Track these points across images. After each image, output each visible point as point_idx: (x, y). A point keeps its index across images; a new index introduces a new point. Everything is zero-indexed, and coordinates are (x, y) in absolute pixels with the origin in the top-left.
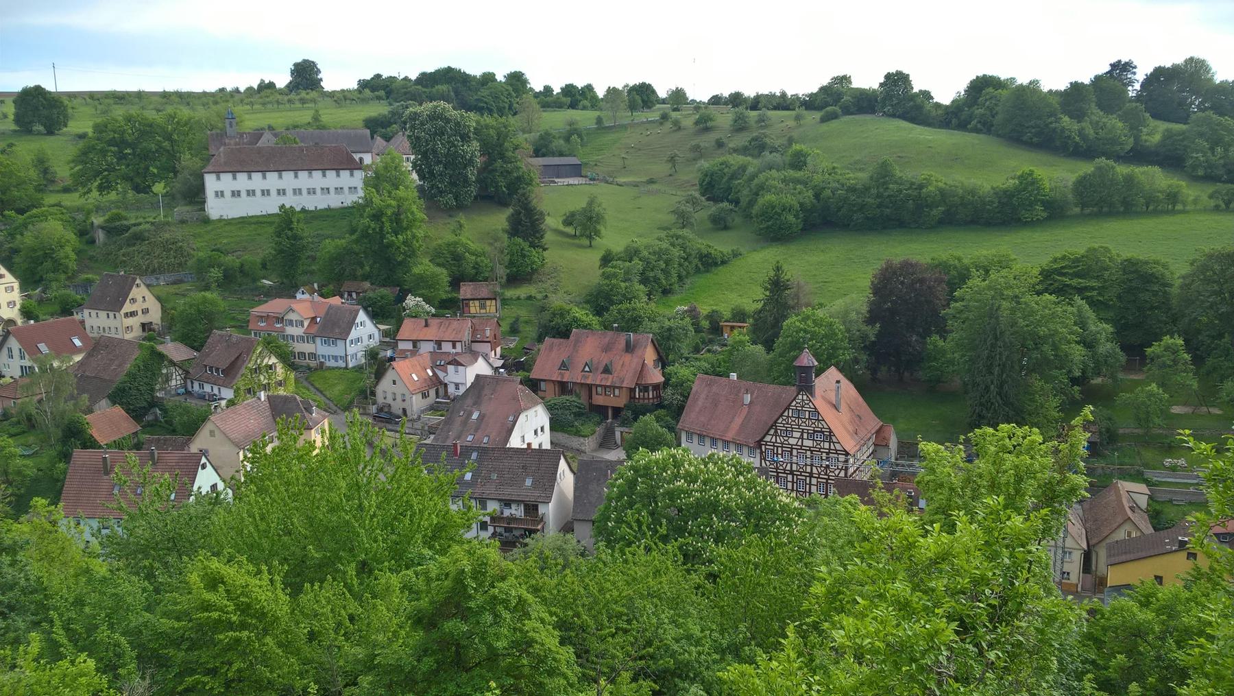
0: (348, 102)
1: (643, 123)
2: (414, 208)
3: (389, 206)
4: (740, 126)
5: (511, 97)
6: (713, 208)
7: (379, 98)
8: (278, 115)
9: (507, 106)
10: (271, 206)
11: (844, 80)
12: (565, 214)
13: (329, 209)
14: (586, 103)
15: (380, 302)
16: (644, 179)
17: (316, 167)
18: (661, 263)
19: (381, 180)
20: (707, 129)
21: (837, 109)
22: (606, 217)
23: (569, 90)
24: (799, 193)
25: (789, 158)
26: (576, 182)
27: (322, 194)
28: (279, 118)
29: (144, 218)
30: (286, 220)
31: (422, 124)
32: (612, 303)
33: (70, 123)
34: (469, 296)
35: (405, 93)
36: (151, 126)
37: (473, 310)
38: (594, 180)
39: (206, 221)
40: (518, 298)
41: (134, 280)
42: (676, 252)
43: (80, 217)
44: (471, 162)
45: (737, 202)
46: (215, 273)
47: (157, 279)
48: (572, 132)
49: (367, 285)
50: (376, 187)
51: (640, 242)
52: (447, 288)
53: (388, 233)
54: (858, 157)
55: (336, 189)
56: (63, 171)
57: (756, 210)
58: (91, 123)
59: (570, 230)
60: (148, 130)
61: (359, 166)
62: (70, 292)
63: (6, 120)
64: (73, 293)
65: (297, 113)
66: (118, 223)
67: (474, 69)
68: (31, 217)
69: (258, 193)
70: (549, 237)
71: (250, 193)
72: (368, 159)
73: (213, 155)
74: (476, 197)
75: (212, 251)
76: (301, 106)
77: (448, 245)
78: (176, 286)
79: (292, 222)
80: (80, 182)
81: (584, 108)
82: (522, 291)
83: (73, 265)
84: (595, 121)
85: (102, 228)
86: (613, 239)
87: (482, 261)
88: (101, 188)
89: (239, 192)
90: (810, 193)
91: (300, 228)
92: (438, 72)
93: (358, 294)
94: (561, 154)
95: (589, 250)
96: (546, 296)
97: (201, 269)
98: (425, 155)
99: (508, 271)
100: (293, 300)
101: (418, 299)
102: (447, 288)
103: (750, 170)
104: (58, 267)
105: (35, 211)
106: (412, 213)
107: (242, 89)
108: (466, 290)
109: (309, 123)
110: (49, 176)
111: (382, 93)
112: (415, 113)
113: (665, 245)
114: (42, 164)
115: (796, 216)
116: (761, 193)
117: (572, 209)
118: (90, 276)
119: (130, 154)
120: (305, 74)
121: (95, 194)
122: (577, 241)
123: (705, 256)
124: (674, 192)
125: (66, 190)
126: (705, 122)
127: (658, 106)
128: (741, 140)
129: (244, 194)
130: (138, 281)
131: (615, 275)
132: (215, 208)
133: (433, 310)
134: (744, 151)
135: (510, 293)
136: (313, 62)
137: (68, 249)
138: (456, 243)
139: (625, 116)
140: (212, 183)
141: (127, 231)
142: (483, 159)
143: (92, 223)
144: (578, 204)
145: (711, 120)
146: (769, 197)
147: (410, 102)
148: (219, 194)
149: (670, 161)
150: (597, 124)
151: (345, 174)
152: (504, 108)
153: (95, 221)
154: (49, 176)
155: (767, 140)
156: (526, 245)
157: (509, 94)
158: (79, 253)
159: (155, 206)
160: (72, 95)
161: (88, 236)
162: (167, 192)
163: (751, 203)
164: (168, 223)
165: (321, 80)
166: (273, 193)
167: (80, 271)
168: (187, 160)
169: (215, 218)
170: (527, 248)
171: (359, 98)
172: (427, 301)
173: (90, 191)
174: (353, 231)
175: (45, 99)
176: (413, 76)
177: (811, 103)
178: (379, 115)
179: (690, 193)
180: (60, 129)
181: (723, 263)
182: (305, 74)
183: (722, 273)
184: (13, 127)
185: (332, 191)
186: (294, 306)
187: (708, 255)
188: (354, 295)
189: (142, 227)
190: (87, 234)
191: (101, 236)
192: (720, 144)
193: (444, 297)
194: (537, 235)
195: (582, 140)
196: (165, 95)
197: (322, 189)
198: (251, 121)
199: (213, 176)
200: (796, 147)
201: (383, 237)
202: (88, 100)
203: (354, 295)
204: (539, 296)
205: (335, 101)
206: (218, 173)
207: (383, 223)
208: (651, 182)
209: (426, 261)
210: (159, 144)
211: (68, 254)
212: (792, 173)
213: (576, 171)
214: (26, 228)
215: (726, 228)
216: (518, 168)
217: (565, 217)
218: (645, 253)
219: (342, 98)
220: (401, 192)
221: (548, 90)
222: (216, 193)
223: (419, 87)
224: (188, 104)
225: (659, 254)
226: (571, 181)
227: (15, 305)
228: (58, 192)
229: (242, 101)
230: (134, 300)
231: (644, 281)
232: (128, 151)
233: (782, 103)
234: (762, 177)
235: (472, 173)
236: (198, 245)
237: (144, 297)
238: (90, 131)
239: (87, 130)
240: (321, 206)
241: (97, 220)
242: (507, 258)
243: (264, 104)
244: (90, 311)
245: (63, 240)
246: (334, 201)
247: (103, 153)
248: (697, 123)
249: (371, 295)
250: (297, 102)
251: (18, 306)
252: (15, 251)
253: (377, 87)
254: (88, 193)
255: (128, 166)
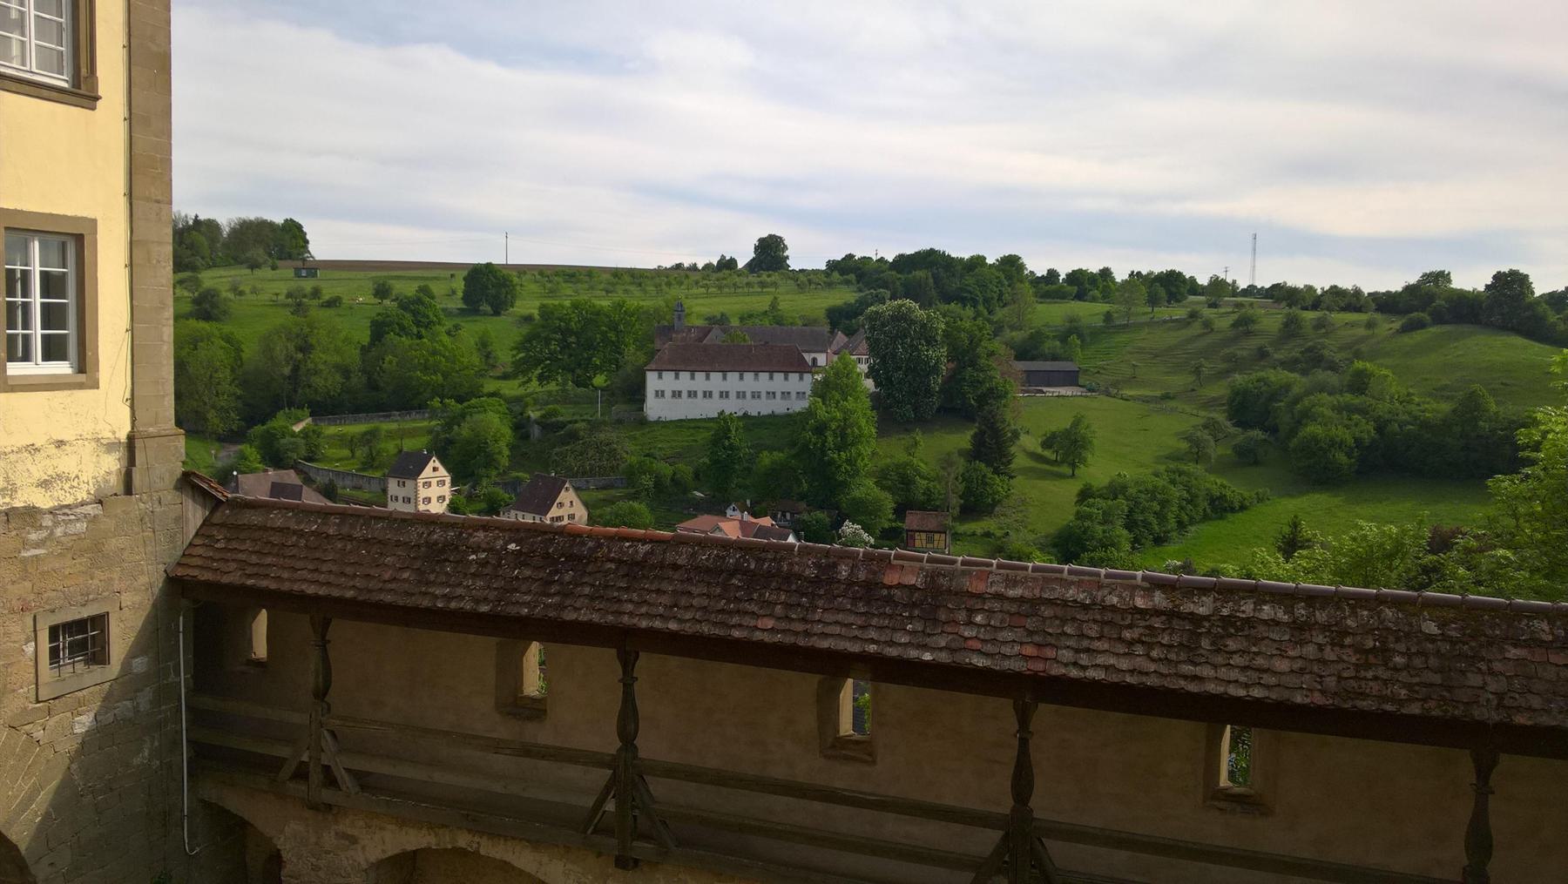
0: (813, 286)
1: (1165, 322)
2: (863, 422)
3: (834, 419)
4: (1291, 329)
5: (1003, 285)
6: (1240, 436)
7: (848, 282)
8: (734, 300)
9: (995, 296)
10: (709, 409)
11: (1441, 277)
12: (1045, 435)
13: (773, 416)
14: (1096, 293)
15: (814, 526)
16: (1158, 393)
17: (763, 369)
18: (1155, 504)
19: (832, 387)
20: (1248, 334)
21: (1425, 316)
22: (1095, 441)
23: (1076, 277)
24: (1356, 425)
25: (1349, 378)
26: (1069, 393)
27: (768, 398)
28: (730, 305)
29: (581, 416)
30: (722, 424)
31: (883, 325)
32: (1085, 549)
33: (518, 303)
34: (915, 527)
35: (877, 280)
36: (598, 314)
37: (918, 543)
38: (1093, 391)
39: (643, 422)
40: (974, 534)
41: (564, 483)
42: (1176, 492)
43: (517, 409)
44: (935, 370)
45: (1274, 430)
46: (647, 481)
47: (588, 482)
48: (1072, 331)
49: (803, 505)
50: (823, 397)
51: (1129, 473)
52: (890, 516)
53: (829, 449)
54: (1445, 382)
55: (783, 393)
56: (505, 357)
57: (1294, 443)
58: (537, 303)
59: (1048, 454)
60: (592, 318)
61: (812, 368)
62: (499, 491)
63: (454, 297)
64: (501, 492)
65: (754, 299)
66: (554, 419)
67: (961, 251)
68: (469, 407)
69: (700, 394)
70: (1020, 461)
71: (692, 394)
72: (822, 359)
73: (659, 351)
74: (938, 410)
75: (645, 456)
76: (760, 290)
77: (898, 466)
78: (605, 492)
79: (730, 431)
80: (520, 369)
81: (1094, 300)
82: (977, 527)
83: (505, 462)
84: (1103, 318)
85: (538, 423)
86: (1099, 470)
87: (935, 487)
88: (541, 378)
89: (680, 392)
90: (1371, 427)
91: (736, 437)
92: (918, 254)
93: (792, 515)
94: (1055, 358)
95: (1071, 480)
96: (1007, 534)
97: (631, 476)
98: (883, 359)
99: (962, 501)
100: (723, 518)
101: (855, 526)
102: (890, 516)
103: (1296, 390)
104: (490, 462)
105: (474, 401)
106: (860, 428)
107: (700, 266)
108: (912, 520)
109: (766, 312)
110: (491, 361)
111: (852, 277)
112: (877, 313)
113: (1161, 483)
114: (484, 345)
115: (1349, 455)
116: (1304, 421)
117: (1054, 429)
118: (520, 474)
119: (574, 343)
120: (770, 252)
121: (535, 383)
122: (1055, 469)
123: (1218, 498)
124: (1195, 412)
125: (505, 377)
126: (1246, 324)
127: (1192, 298)
128: (1292, 350)
129: (685, 395)
130: (567, 485)
131: (1089, 517)
132: (654, 408)
133: (872, 541)
134: (1290, 365)
135: (963, 528)
136: (780, 238)
137: (502, 444)
138: (906, 465)
139: (1142, 310)
140: (653, 381)
141: (562, 428)
142: (951, 365)
143: (529, 417)
144: (1061, 422)
145: (1253, 322)
146: (1312, 429)
147: (881, 290)
148: (660, 394)
149: (1194, 372)
150: (1104, 321)
151: (794, 377)
152: (992, 298)
153: (532, 415)
154: (491, 361)
155: (1326, 352)
156: (988, 471)
157: (999, 282)
158: (512, 448)
159: (592, 402)
160: (522, 269)
161: (524, 430)
162: (608, 386)
163: (1293, 432)
164: (604, 423)
165: (787, 257)
166: (716, 395)
167: (510, 468)
168: (632, 355)
169: (652, 420)
170: (989, 475)
171: (825, 283)
172: (866, 528)
173: (530, 380)
174: (793, 444)
175: (495, 277)
176: (890, 258)
177: (1386, 303)
178: (845, 304)
179: (1212, 415)
180: (507, 310)
181: (1243, 508)
182: (770, 252)
183: (1235, 522)
184: (461, 305)
185: (778, 395)
186: (721, 525)
187: (1222, 497)
188: (788, 515)
189: (577, 425)
190: (523, 428)
191: (536, 431)
192: (1262, 354)
193: (886, 526)
194: (1004, 460)
195: (1082, 341)
196: (617, 274)
197: (768, 393)
198: (701, 307)
199: (656, 374)
200: (1359, 365)
201: (824, 453)
202: (538, 277)
203: (788, 515)
204: (999, 533)
205: (798, 285)
206: (660, 371)
207: (826, 437)
208: (1166, 397)
209: (870, 483)
210: (604, 334)
211: (503, 452)
212: (1348, 398)
213: (1071, 379)
214: (464, 418)
215: (1256, 463)
216: (992, 378)
217: (1045, 438)
218: (1132, 491)
219: (806, 280)
220: (850, 404)
221: (1052, 274)
222: (705, 392)
223: (894, 273)
224: (640, 285)
225: (1152, 493)
226: (1063, 391)
227: (444, 500)
228: (498, 378)
229: (697, 283)
230: (561, 505)
231: (1130, 525)
232: (573, 339)
233: (1345, 300)
234: (1306, 402)
235: (936, 382)
236: (633, 448)
237: (571, 502)
238: (536, 312)
239: (533, 311)
240: (765, 411)
241: (534, 414)
242: (961, 487)
243: (720, 288)
244: (517, 512)
245: (498, 435)
246: (779, 407)
247: (547, 341)
248: (1235, 325)
249: (805, 518)
250: (756, 286)
251: (447, 502)
252: (450, 442)
253: (848, 269)
254: (528, 382)
255: (571, 355)
